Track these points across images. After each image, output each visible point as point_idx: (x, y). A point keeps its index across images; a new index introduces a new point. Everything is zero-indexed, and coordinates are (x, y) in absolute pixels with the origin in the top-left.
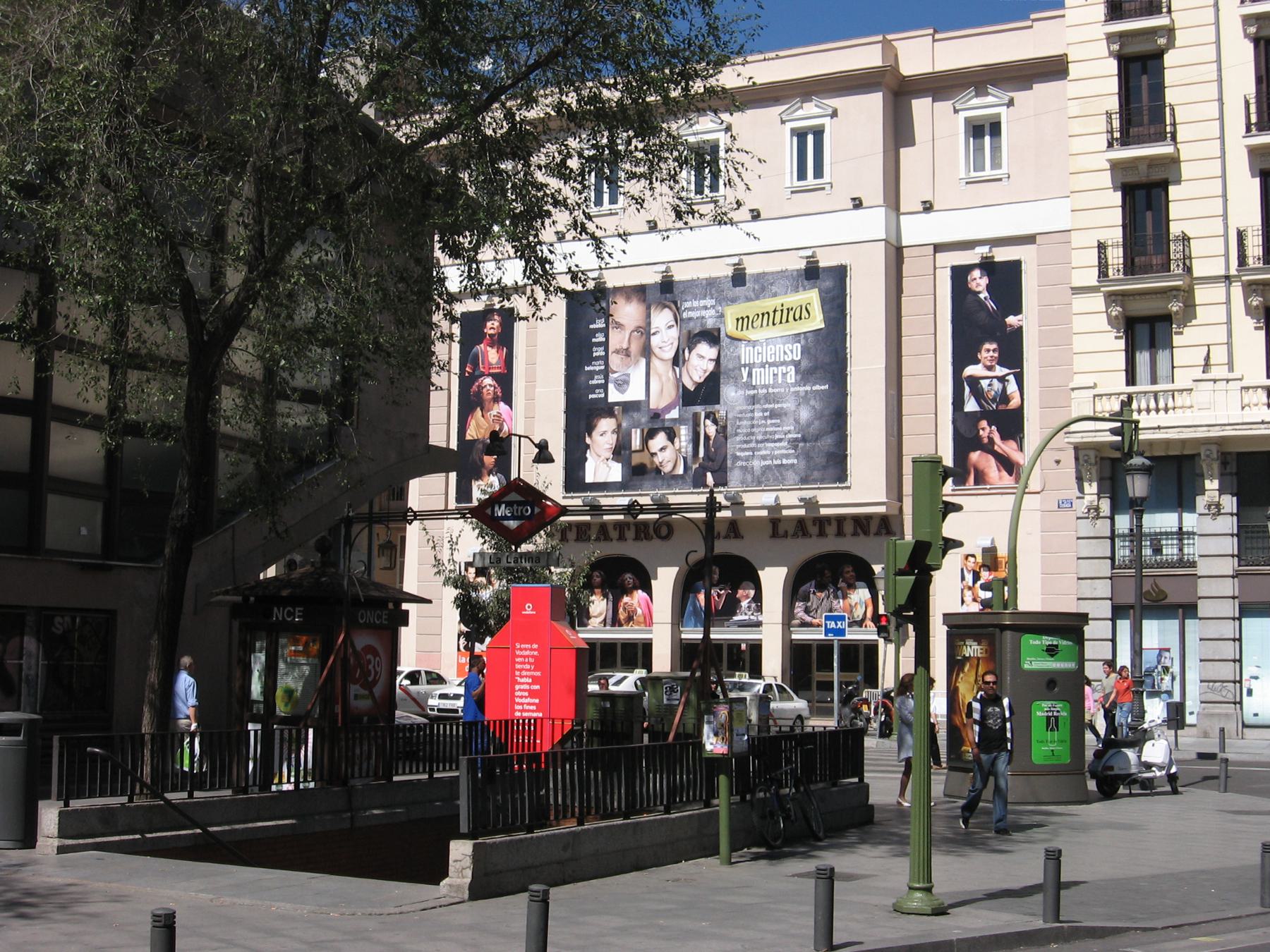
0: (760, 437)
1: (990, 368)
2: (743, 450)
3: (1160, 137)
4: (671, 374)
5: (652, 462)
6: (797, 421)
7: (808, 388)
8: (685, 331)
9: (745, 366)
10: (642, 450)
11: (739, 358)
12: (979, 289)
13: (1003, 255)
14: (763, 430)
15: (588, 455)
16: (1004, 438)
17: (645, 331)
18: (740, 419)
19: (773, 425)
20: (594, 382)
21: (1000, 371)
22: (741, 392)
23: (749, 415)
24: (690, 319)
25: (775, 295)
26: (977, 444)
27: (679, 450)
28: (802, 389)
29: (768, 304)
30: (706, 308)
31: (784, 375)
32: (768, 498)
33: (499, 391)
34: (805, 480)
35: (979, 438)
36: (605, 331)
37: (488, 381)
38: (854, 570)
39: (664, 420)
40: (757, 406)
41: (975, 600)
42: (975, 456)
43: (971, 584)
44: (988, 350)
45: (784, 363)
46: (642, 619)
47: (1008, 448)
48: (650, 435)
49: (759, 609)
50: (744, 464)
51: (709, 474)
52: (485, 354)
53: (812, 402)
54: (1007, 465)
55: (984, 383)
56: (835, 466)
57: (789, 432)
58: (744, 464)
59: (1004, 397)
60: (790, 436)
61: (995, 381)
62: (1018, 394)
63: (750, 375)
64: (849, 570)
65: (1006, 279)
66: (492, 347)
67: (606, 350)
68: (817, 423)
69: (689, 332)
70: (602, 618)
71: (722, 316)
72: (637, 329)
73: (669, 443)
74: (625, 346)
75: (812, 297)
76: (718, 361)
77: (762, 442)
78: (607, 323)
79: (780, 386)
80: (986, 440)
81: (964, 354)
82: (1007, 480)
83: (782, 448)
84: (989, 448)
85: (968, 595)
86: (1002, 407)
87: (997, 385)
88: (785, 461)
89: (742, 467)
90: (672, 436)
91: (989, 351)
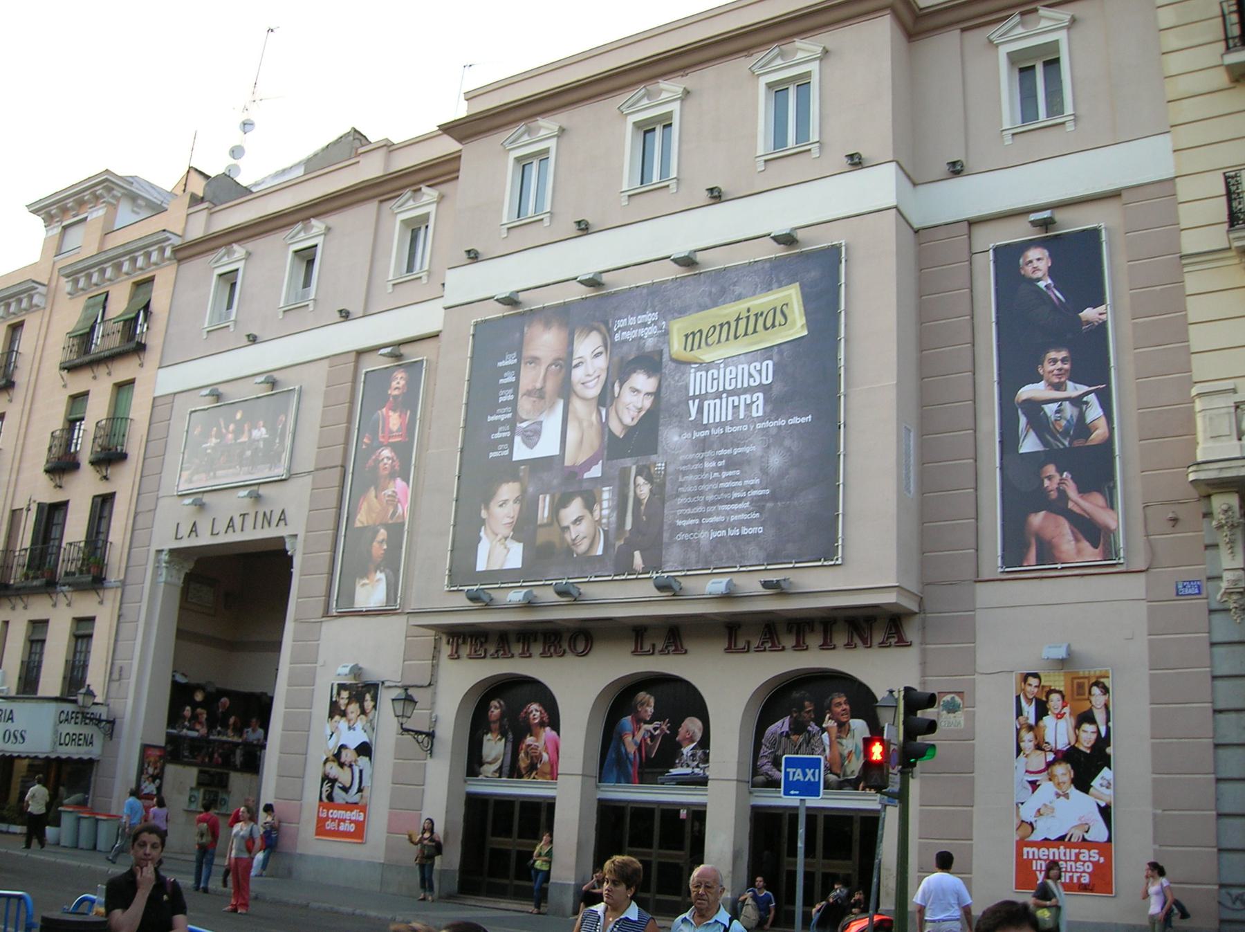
0: (710, 498)
1: (1058, 387)
2: (686, 517)
3: (678, 894)
4: (594, 417)
5: (563, 539)
6: (764, 471)
7: (782, 422)
8: (616, 359)
9: (694, 398)
10: (550, 524)
11: (687, 388)
12: (1039, 274)
13: (1074, 222)
14: (715, 486)
15: (482, 534)
16: (1083, 490)
17: (566, 363)
18: (685, 473)
19: (729, 478)
20: (498, 435)
21: (1074, 390)
22: (687, 435)
23: (696, 466)
24: (625, 342)
25: (739, 298)
26: (1041, 500)
27: (599, 522)
28: (772, 424)
29: (729, 311)
30: (645, 325)
31: (749, 406)
32: (717, 585)
33: (397, 463)
34: (773, 558)
35: (1045, 492)
36: (516, 369)
37: (386, 453)
38: (848, 702)
39: (582, 480)
40: (709, 453)
41: (1038, 747)
42: (1037, 519)
43: (1032, 721)
44: (1055, 361)
45: (750, 390)
46: (547, 769)
47: (1092, 505)
48: (560, 503)
49: (706, 759)
50: (687, 536)
51: (637, 554)
52: (386, 419)
53: (787, 443)
54: (1091, 531)
55: (1050, 409)
56: (821, 538)
57: (753, 487)
58: (687, 536)
59: (1082, 428)
60: (754, 493)
61: (1067, 404)
62: (1102, 423)
63: (700, 410)
64: (840, 702)
65: (1078, 257)
66: (395, 411)
67: (516, 393)
68: (793, 472)
69: (622, 358)
70: (496, 766)
71: (666, 333)
72: (555, 362)
73: (586, 512)
74: (538, 385)
75: (792, 295)
76: (657, 394)
77: (713, 503)
78: (519, 358)
79: (741, 422)
80: (1054, 495)
81: (1018, 366)
82: (1090, 554)
83: (740, 511)
84: (1059, 506)
85: (1028, 738)
86: (1076, 444)
87: (1069, 411)
88: (745, 531)
89: (684, 541)
90: (591, 502)
91: (1056, 360)
